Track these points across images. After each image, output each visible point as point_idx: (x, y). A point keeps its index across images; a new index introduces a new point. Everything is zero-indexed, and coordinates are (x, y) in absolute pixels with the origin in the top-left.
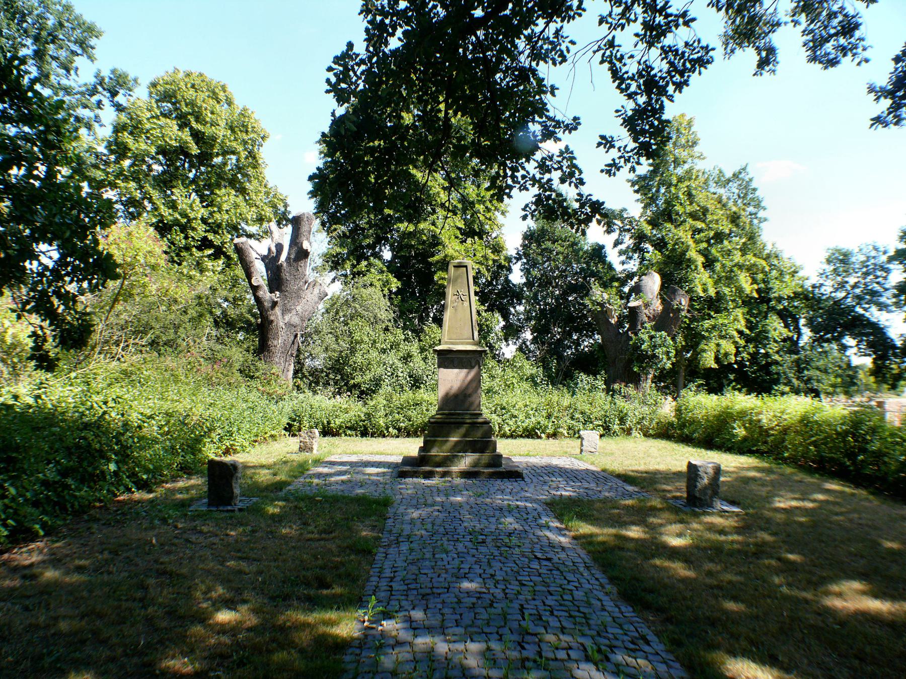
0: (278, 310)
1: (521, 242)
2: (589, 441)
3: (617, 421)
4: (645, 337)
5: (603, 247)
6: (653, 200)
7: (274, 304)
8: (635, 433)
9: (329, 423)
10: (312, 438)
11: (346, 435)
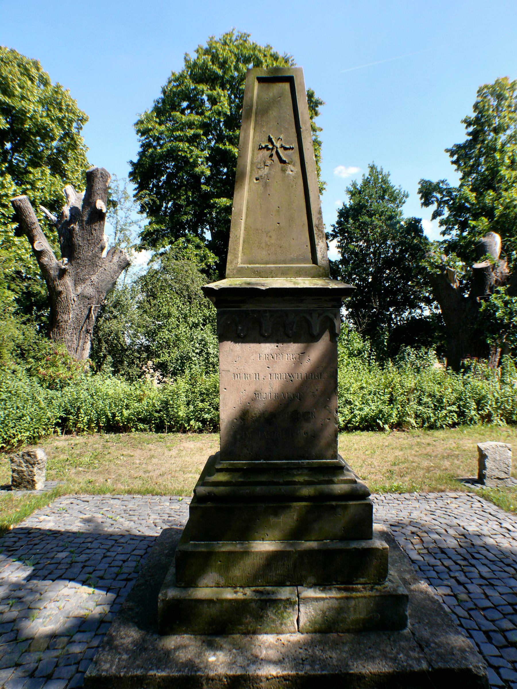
0: (68, 280)
1: (337, 219)
2: (495, 460)
3: (474, 405)
4: (499, 303)
5: (419, 221)
6: (474, 168)
7: (62, 273)
8: (496, 420)
9: (114, 415)
10: (33, 464)
11: (137, 430)
